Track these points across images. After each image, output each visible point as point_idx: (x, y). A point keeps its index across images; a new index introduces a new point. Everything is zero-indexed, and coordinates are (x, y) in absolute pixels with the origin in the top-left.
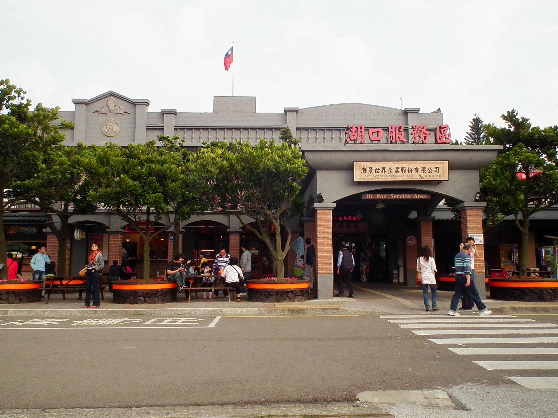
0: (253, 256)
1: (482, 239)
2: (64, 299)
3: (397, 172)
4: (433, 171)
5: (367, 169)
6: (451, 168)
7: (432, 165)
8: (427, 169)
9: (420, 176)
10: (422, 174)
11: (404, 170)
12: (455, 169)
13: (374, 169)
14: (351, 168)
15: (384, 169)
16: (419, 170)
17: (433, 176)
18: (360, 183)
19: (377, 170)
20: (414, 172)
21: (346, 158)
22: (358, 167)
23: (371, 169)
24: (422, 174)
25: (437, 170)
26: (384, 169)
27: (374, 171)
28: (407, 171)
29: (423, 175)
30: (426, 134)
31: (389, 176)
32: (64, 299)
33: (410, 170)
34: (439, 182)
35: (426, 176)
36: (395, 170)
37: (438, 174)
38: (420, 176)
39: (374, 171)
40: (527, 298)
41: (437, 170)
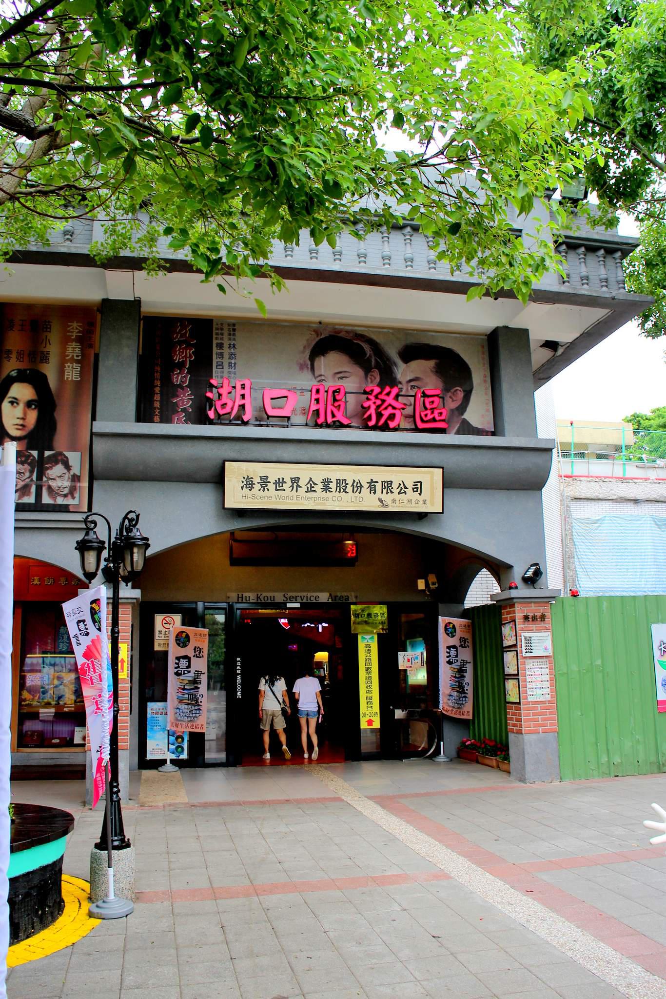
0: (438, 707)
1: (549, 643)
2: (516, 676)
3: (326, 489)
4: (409, 491)
5: (257, 480)
6: (447, 484)
7: (409, 476)
8: (395, 485)
9: (380, 500)
10: (384, 497)
11: (342, 485)
12: (461, 488)
13: (272, 479)
14: (218, 480)
15: (295, 480)
16: (379, 487)
17: (410, 501)
18: (240, 513)
19: (280, 483)
20: (365, 490)
21: (211, 453)
22: (234, 473)
23: (264, 481)
24: (384, 497)
25: (418, 487)
26: (295, 480)
27: (271, 486)
28: (349, 489)
29: (387, 498)
30: (394, 408)
31: (308, 499)
32: (516, 676)
33: (358, 487)
34: (421, 516)
35: (394, 501)
36: (321, 486)
37: (421, 498)
38: (380, 500)
39: (271, 486)
40: (20, 611)
41: (418, 487)
